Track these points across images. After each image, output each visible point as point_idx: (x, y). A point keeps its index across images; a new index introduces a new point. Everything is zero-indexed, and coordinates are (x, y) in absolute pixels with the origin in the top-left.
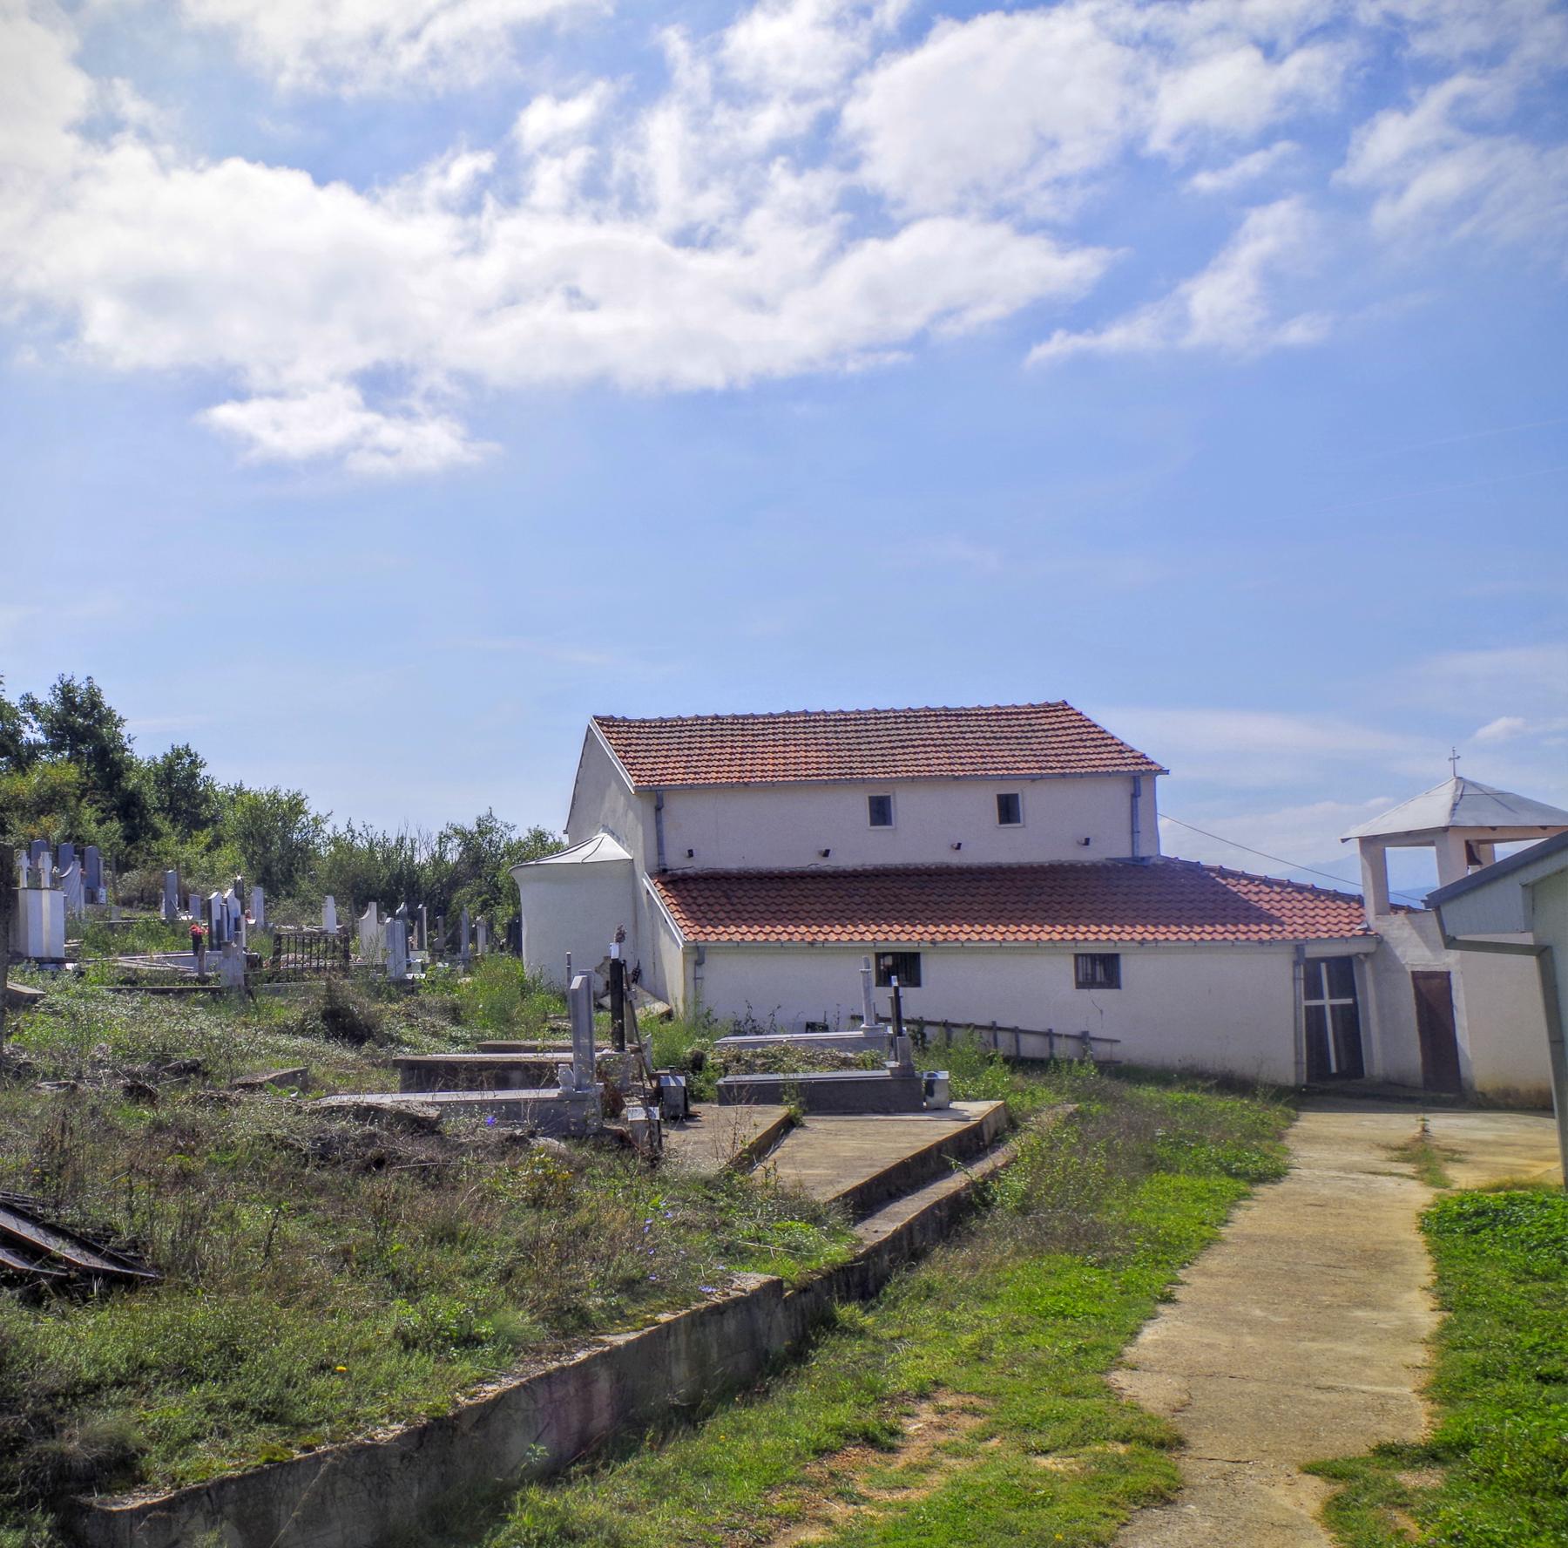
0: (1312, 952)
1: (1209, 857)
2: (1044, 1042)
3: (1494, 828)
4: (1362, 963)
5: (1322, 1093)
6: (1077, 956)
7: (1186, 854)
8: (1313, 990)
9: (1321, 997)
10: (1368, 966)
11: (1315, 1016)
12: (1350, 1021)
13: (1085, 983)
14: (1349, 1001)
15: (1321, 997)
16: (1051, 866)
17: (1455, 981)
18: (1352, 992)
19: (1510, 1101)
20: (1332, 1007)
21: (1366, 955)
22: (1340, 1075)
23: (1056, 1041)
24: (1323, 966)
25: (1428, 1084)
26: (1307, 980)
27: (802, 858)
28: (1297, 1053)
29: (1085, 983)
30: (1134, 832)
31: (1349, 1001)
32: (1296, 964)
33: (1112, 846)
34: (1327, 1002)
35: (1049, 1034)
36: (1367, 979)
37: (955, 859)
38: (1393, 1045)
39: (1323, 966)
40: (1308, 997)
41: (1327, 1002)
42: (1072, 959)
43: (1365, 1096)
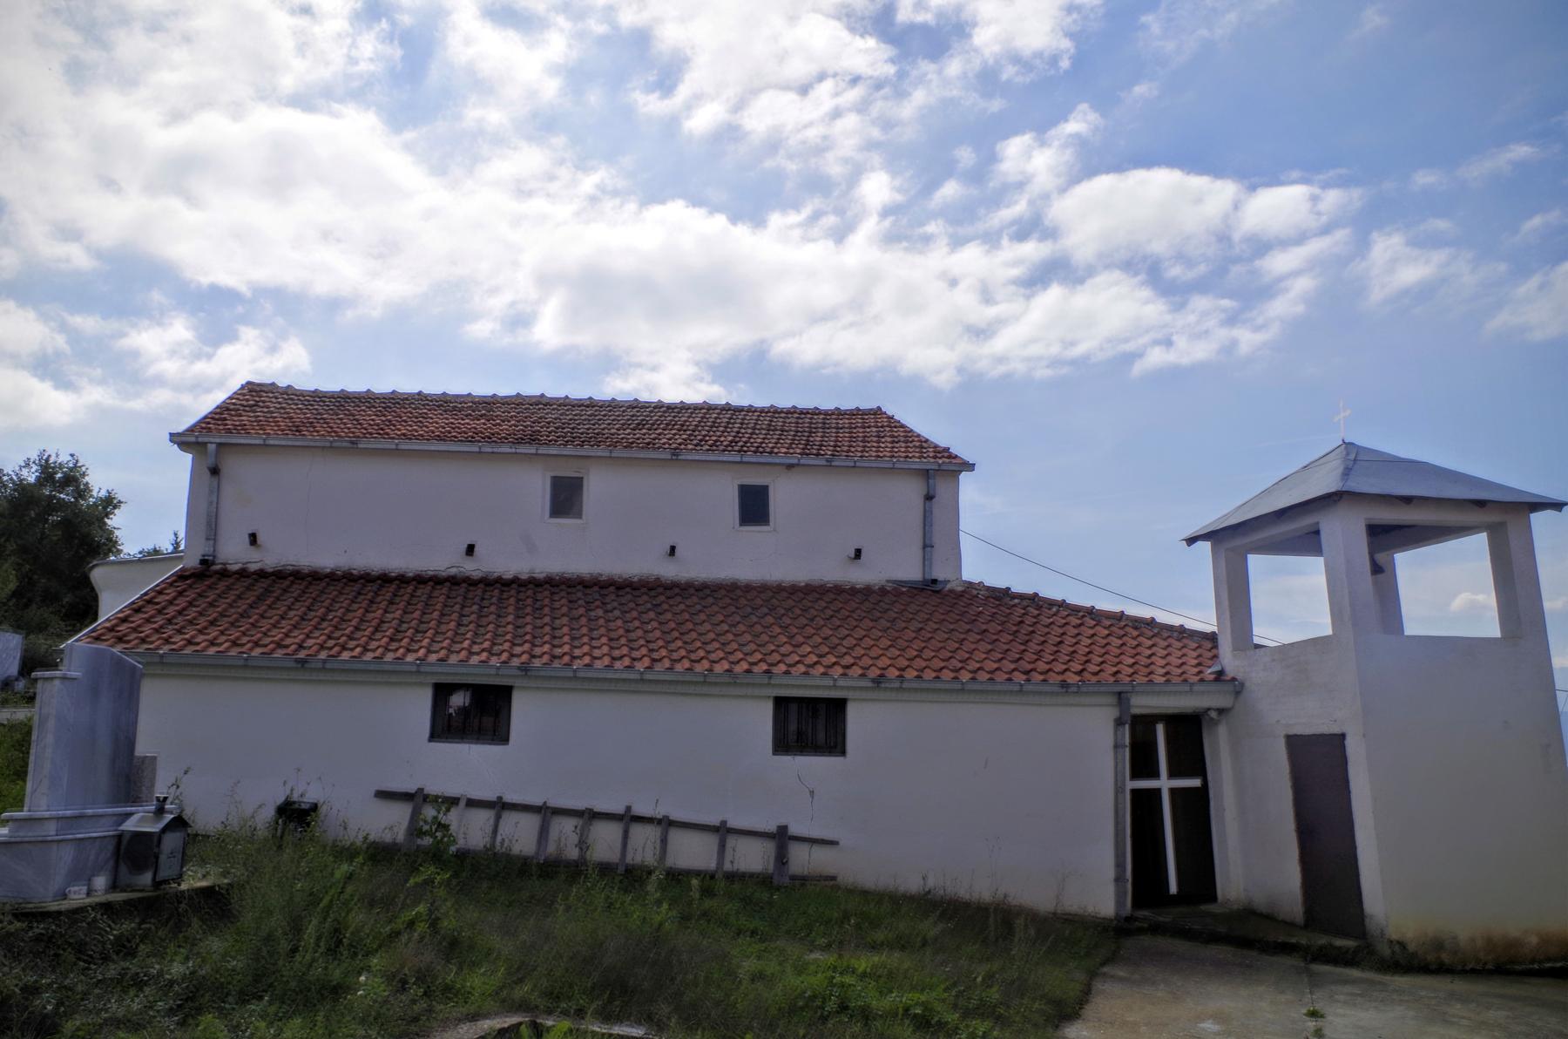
0: (1143, 703)
1: (1021, 582)
2: (711, 841)
3: (1407, 500)
4: (1214, 723)
5: (1156, 929)
6: (781, 703)
7: (996, 578)
8: (1143, 763)
9: (1155, 774)
10: (1222, 731)
11: (1145, 804)
12: (1196, 810)
13: (785, 743)
14: (1195, 783)
15: (1155, 774)
16: (807, 585)
17: (1354, 748)
18: (1199, 769)
19: (1446, 957)
20: (1173, 791)
21: (1221, 711)
22: (1182, 898)
23: (731, 841)
24: (1160, 730)
25: (1312, 920)
26: (1135, 747)
27: (442, 559)
28: (1120, 865)
29: (785, 743)
30: (927, 546)
31: (1195, 783)
32: (1119, 723)
33: (896, 564)
34: (1164, 783)
35: (722, 831)
36: (1219, 748)
37: (669, 571)
38: (1256, 859)
39: (1160, 730)
40: (1135, 775)
41: (1164, 783)
42: (768, 708)
43: (1213, 938)
